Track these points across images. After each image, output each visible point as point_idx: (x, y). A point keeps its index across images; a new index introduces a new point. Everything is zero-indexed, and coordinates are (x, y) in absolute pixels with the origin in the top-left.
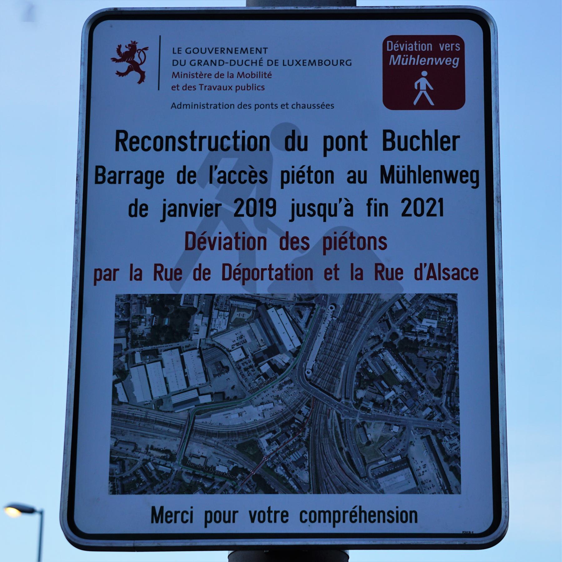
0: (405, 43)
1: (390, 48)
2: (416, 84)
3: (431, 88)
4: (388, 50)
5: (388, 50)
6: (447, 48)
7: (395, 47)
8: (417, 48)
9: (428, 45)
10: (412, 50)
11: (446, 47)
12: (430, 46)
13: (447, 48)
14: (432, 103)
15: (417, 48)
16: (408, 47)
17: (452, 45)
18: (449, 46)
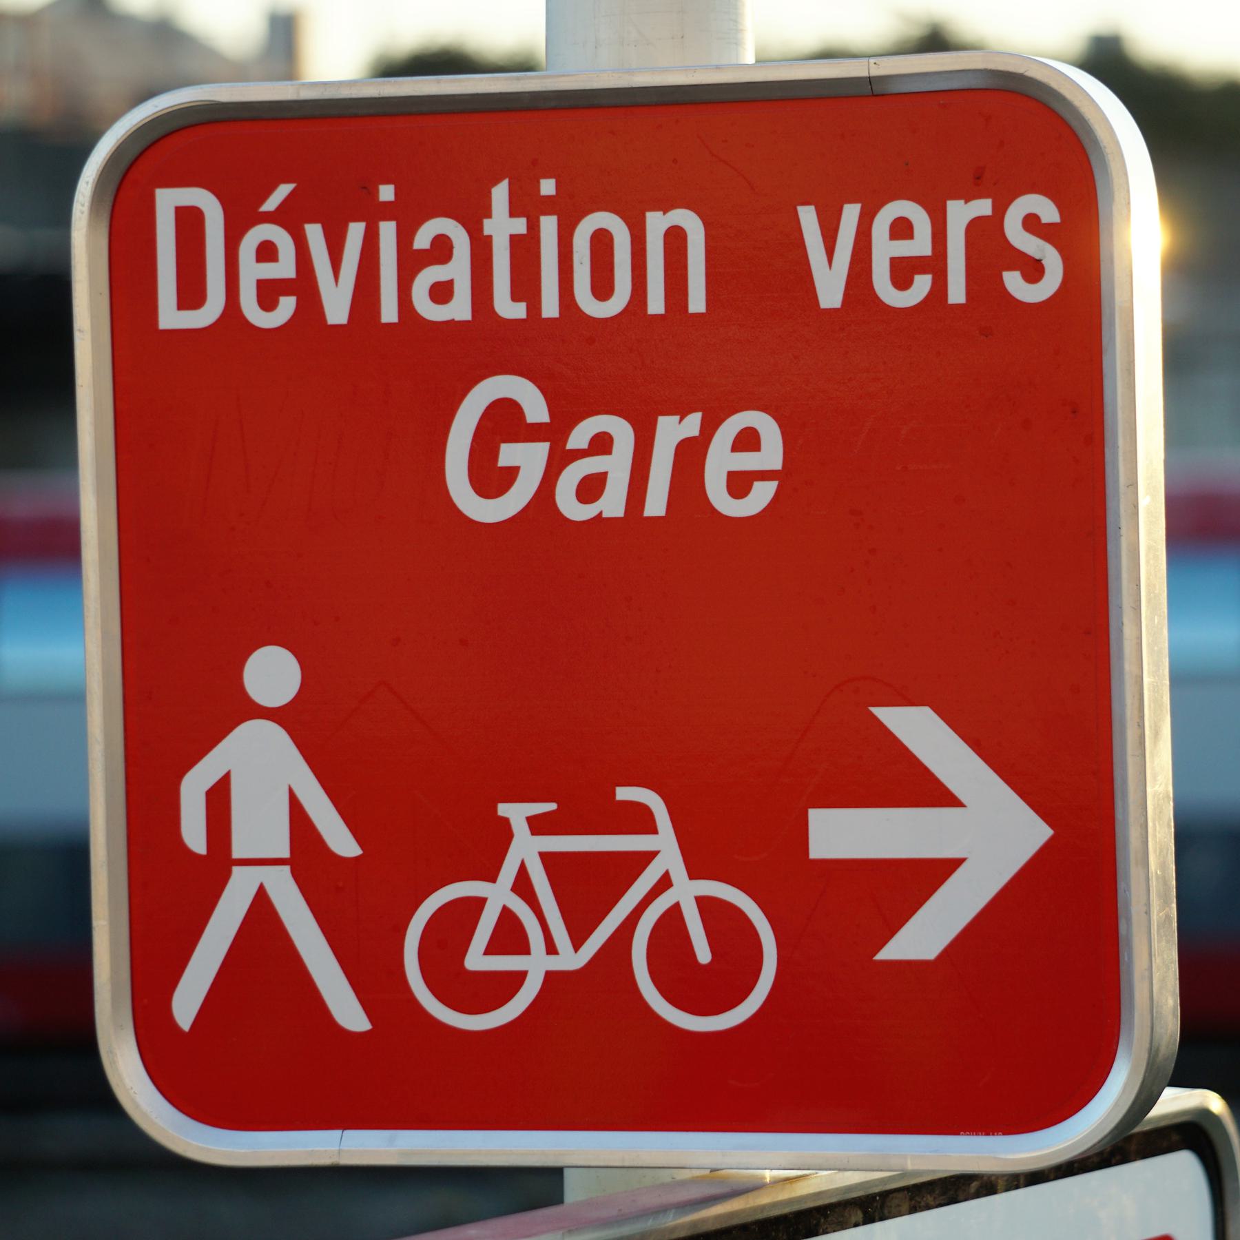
0: (374, 214)
1: (191, 296)
2: (193, 790)
3: (342, 842)
4: (170, 317)
5: (170, 317)
6: (903, 272)
7: (251, 272)
8: (526, 284)
9: (657, 224)
10: (460, 309)
11: (884, 249)
12: (675, 240)
13: (903, 272)
14: (187, 1003)
15: (526, 284)
16: (410, 262)
17: (960, 214)
18: (920, 245)
